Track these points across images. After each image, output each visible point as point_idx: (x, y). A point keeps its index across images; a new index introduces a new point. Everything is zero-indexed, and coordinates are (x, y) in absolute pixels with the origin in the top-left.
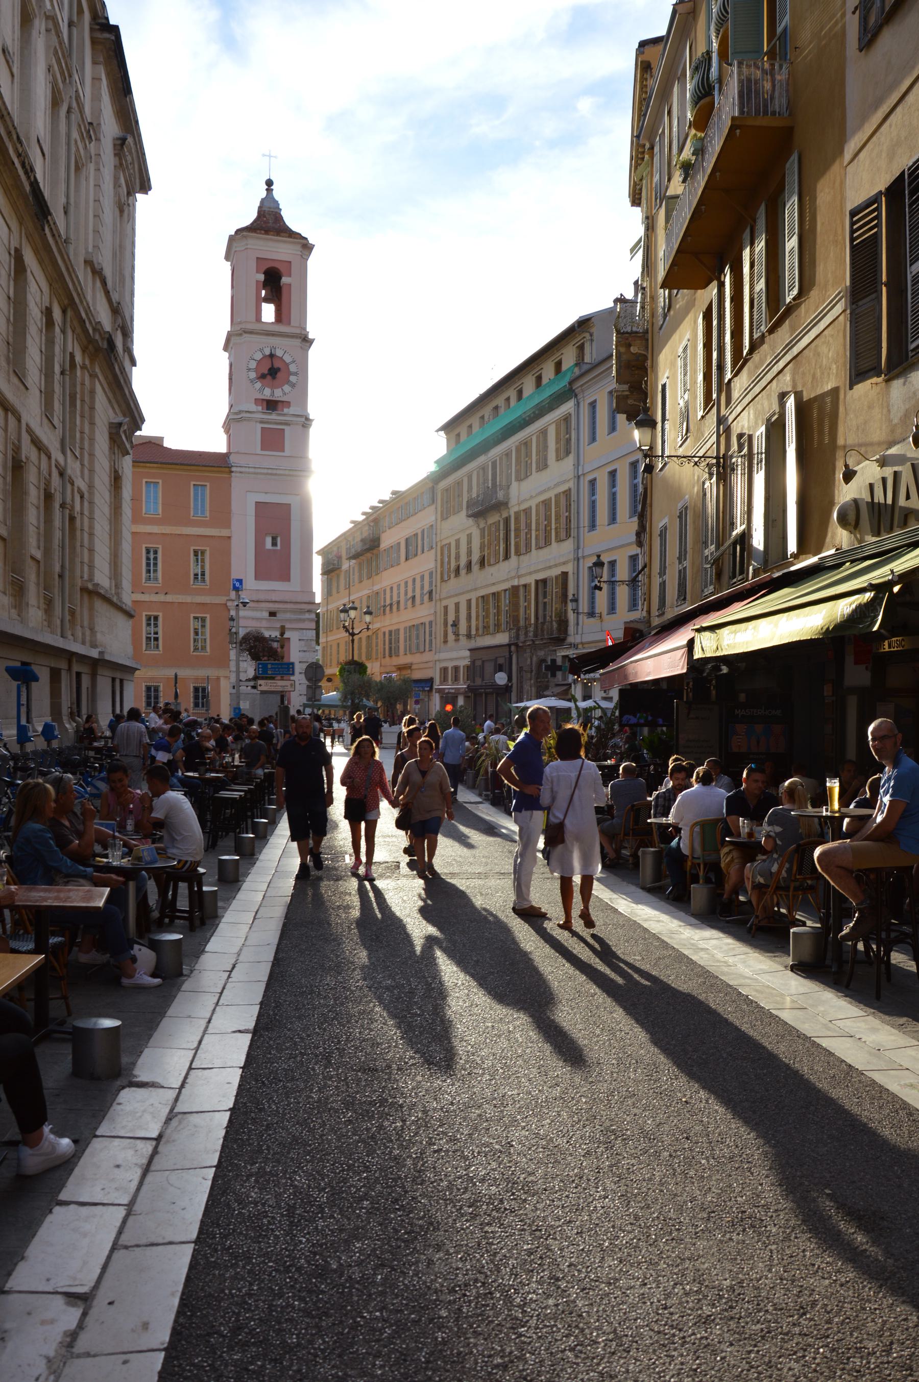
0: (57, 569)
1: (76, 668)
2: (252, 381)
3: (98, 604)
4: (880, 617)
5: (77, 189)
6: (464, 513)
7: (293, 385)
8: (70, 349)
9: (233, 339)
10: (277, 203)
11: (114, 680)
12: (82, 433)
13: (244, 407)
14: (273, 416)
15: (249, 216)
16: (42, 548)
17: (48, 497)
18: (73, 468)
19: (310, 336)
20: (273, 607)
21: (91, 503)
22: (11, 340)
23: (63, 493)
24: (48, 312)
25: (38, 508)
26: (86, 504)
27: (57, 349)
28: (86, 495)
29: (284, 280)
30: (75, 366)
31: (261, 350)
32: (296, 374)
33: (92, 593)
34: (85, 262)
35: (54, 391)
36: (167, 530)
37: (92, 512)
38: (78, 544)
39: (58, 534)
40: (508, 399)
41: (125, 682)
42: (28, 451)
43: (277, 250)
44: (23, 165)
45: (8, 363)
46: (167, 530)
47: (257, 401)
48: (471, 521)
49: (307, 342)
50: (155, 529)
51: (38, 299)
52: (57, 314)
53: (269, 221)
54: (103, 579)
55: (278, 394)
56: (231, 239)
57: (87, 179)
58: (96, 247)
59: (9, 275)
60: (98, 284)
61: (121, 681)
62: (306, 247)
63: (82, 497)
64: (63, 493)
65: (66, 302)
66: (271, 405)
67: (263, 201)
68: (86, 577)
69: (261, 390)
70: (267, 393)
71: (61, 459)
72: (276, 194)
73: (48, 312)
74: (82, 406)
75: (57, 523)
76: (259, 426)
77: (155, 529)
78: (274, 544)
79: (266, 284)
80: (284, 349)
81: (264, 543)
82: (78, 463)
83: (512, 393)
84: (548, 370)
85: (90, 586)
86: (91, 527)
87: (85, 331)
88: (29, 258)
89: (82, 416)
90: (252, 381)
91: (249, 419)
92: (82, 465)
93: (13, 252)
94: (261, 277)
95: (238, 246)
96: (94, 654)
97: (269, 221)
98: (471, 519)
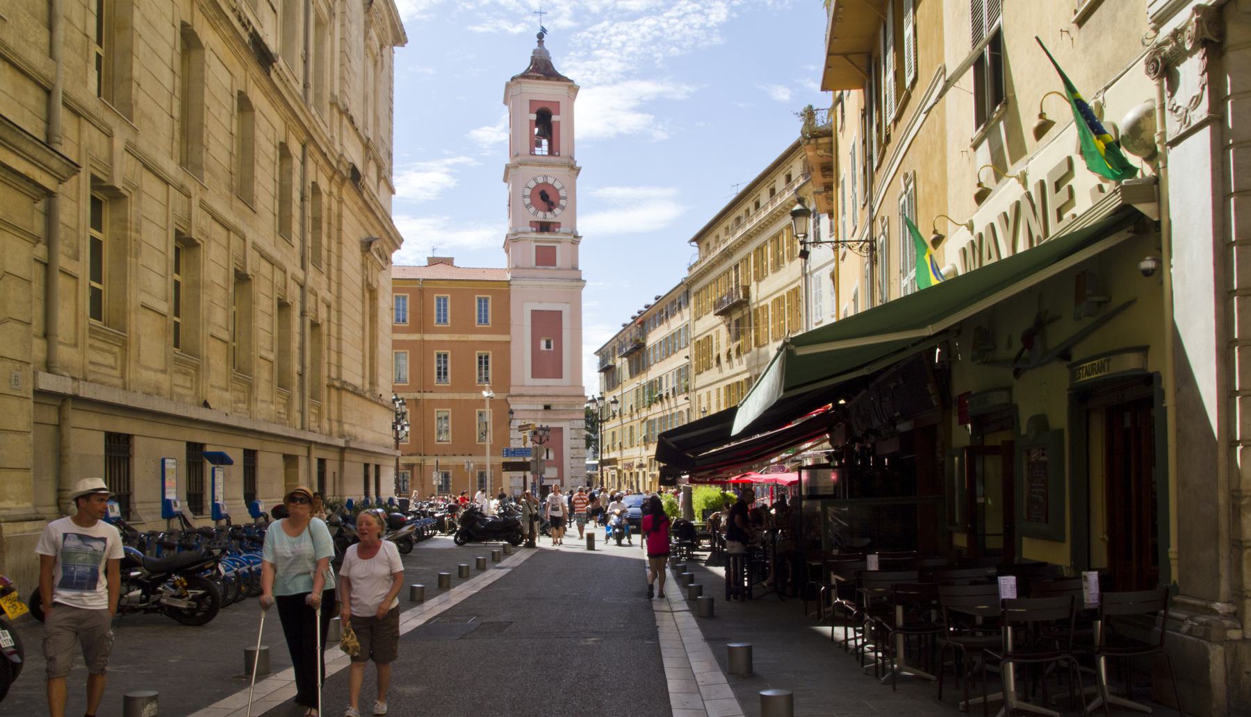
0: (296, 367)
1: (316, 454)
2: (527, 206)
3: (348, 398)
4: (769, 433)
5: (320, 44)
6: (712, 313)
7: (563, 208)
8: (311, 177)
9: (511, 170)
10: (547, 52)
11: (366, 466)
12: (329, 251)
13: (520, 229)
14: (546, 236)
15: (524, 64)
16: (276, 350)
17: (283, 306)
18: (313, 278)
19: (578, 165)
20: (548, 401)
21: (339, 312)
22: (234, 170)
23: (303, 302)
24: (284, 149)
25: (271, 316)
26: (334, 313)
27: (296, 179)
28: (334, 305)
29: (554, 118)
30: (320, 193)
31: (535, 179)
32: (565, 198)
33: (344, 388)
34: (331, 104)
35: (291, 215)
36: (456, 337)
37: (339, 319)
38: (325, 347)
39: (296, 340)
40: (748, 211)
41: (382, 469)
42: (254, 264)
43: (544, 91)
44: (240, 19)
45: (231, 191)
46: (456, 337)
47: (532, 224)
48: (719, 319)
49: (574, 170)
50: (445, 337)
51: (270, 135)
52: (295, 148)
53: (542, 69)
54: (353, 375)
55: (550, 217)
56: (508, 85)
57: (332, 34)
58: (342, 91)
59: (232, 115)
60: (346, 122)
61: (377, 467)
62: (573, 88)
63: (329, 307)
64: (303, 302)
65: (304, 138)
66: (544, 227)
67: (534, 52)
68: (334, 375)
69: (535, 214)
70: (541, 216)
71: (300, 274)
72: (547, 45)
73: (284, 149)
74: (329, 228)
75: (296, 328)
76: (534, 245)
77: (445, 337)
78: (548, 346)
79: (537, 123)
80: (555, 177)
81: (539, 345)
82: (324, 277)
83: (750, 204)
84: (780, 183)
85: (337, 384)
86: (339, 332)
87: (329, 163)
88: (258, 99)
89: (329, 237)
90: (527, 206)
91: (525, 239)
92: (329, 279)
93: (236, 95)
94: (534, 117)
95: (515, 90)
96: (341, 443)
97: (542, 69)
98: (718, 317)
